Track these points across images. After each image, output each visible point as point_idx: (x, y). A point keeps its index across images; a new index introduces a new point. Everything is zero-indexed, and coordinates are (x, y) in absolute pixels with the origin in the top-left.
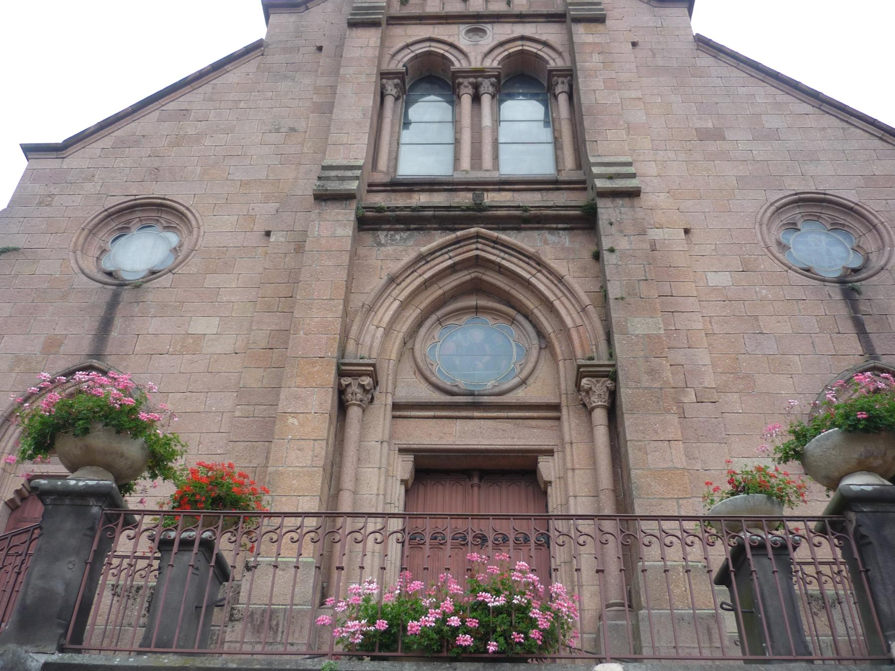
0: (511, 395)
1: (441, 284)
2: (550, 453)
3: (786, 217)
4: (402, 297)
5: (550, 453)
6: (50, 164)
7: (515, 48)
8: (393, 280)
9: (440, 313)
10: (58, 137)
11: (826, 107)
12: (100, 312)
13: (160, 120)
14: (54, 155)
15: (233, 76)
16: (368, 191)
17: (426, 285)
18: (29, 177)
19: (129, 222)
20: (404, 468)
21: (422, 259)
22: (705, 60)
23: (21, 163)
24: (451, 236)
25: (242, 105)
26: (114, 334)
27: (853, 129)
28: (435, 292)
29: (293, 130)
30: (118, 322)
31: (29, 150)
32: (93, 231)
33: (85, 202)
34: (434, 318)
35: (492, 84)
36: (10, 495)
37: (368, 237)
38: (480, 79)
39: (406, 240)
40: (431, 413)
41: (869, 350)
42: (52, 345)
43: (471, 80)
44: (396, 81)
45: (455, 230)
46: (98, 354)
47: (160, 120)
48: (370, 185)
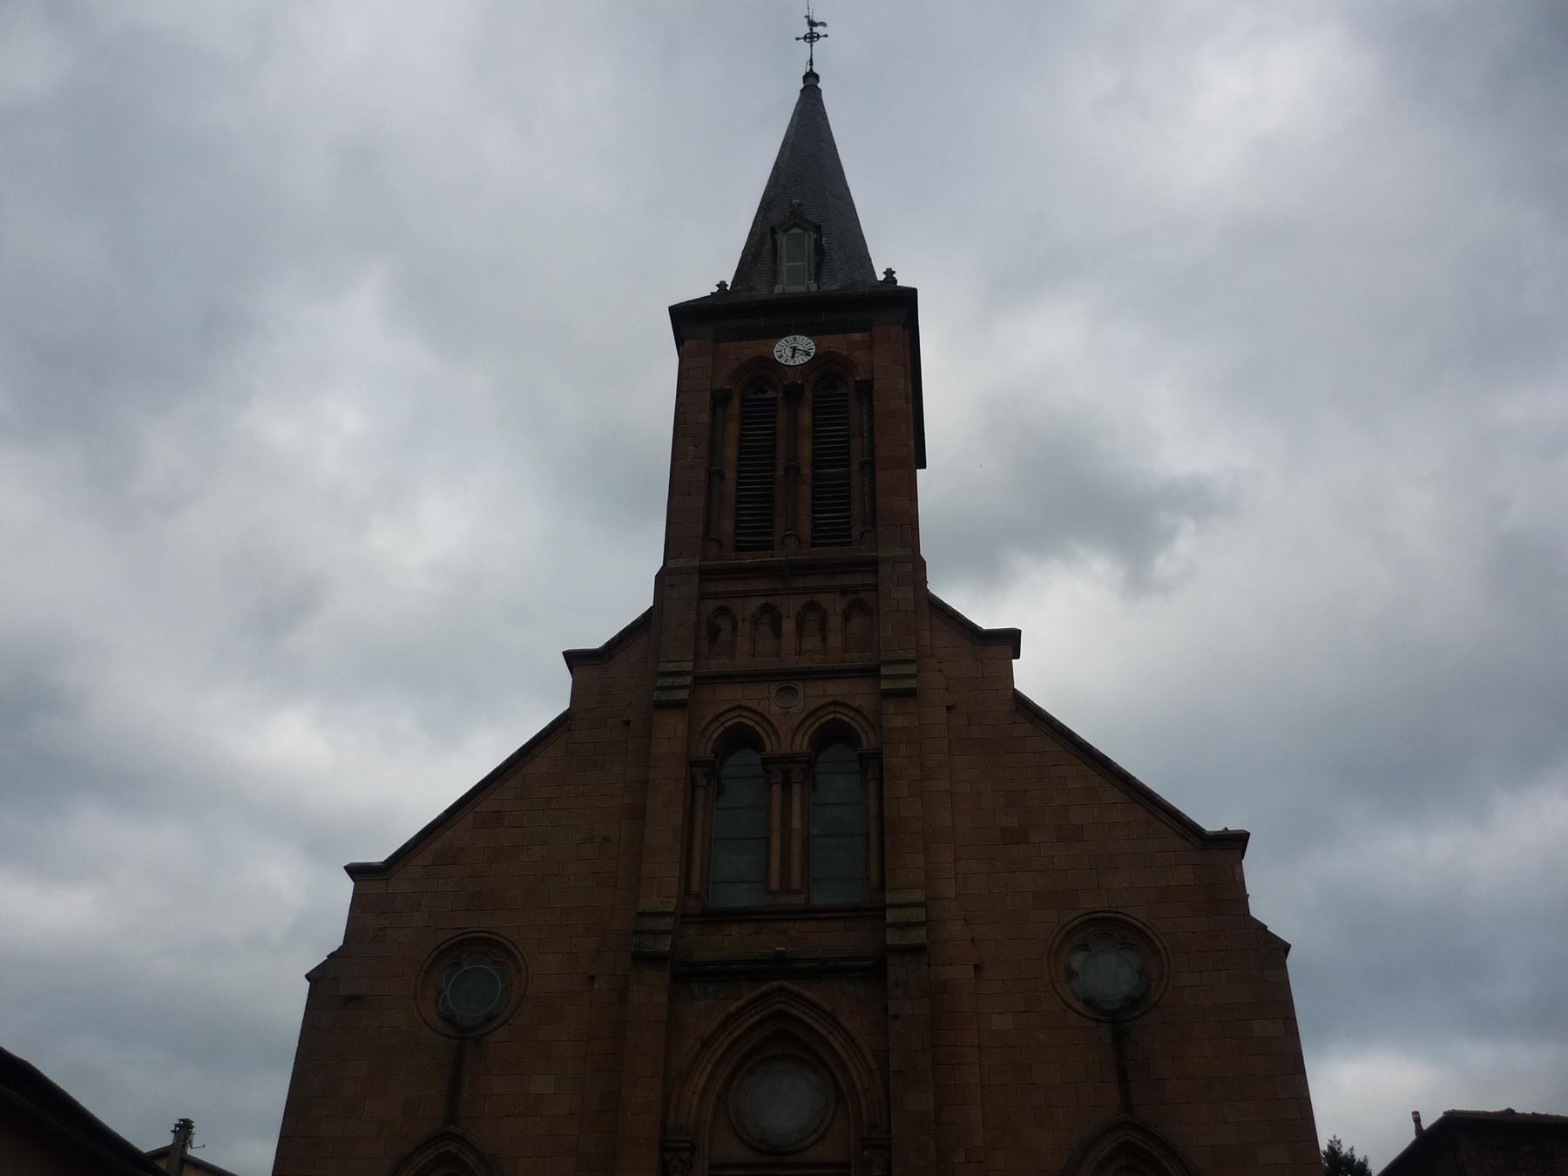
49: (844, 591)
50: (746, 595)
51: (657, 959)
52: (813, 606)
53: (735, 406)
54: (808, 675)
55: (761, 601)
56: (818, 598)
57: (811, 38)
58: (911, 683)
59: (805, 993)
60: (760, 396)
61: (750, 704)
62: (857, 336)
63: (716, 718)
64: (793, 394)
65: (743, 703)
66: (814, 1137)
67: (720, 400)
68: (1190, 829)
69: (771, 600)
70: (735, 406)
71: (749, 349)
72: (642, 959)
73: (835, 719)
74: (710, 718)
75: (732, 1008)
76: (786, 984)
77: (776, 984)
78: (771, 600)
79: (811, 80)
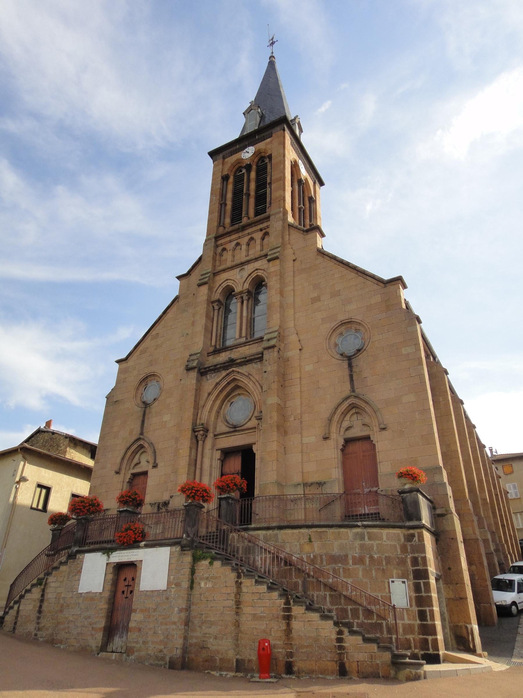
0: (246, 426)
1: (226, 389)
2: (255, 444)
3: (338, 332)
4: (213, 399)
5: (255, 444)
6: (124, 365)
7: (250, 279)
8: (209, 394)
9: (228, 399)
10: (185, 272)
11: (359, 274)
12: (141, 418)
13: (152, 340)
14: (125, 362)
15: (170, 315)
16: (208, 356)
17: (221, 391)
18: (120, 372)
19: (147, 382)
20: (218, 455)
21: (217, 384)
22: (320, 259)
23: (178, 282)
24: (228, 372)
25: (173, 327)
26: (145, 425)
27: (368, 282)
28: (225, 393)
29: (187, 334)
30: (146, 420)
31: (179, 278)
32: (137, 389)
33: (134, 379)
34: (227, 401)
35: (247, 295)
36: (128, 480)
37: (204, 378)
38: (242, 295)
39: (214, 376)
40: (225, 436)
41: (353, 390)
42: (131, 431)
43: (239, 296)
44: (217, 303)
45: (228, 369)
46: (142, 433)
47: (152, 340)
48: (208, 354)
49: (261, 230)
50: (231, 241)
51: (193, 368)
52: (252, 239)
53: (231, 180)
54: (248, 262)
55: (236, 242)
56: (253, 235)
57: (273, 43)
58: (277, 254)
59: (240, 371)
60: (240, 173)
61: (231, 278)
62: (268, 140)
63: (220, 285)
64: (249, 167)
65: (228, 278)
66: (247, 420)
67: (225, 178)
68: (380, 281)
69: (238, 241)
70: (231, 180)
71: (233, 159)
72: (189, 369)
73: (257, 275)
74: (218, 286)
75: (218, 381)
76: (234, 369)
77: (231, 369)
78: (238, 241)
79: (272, 59)
